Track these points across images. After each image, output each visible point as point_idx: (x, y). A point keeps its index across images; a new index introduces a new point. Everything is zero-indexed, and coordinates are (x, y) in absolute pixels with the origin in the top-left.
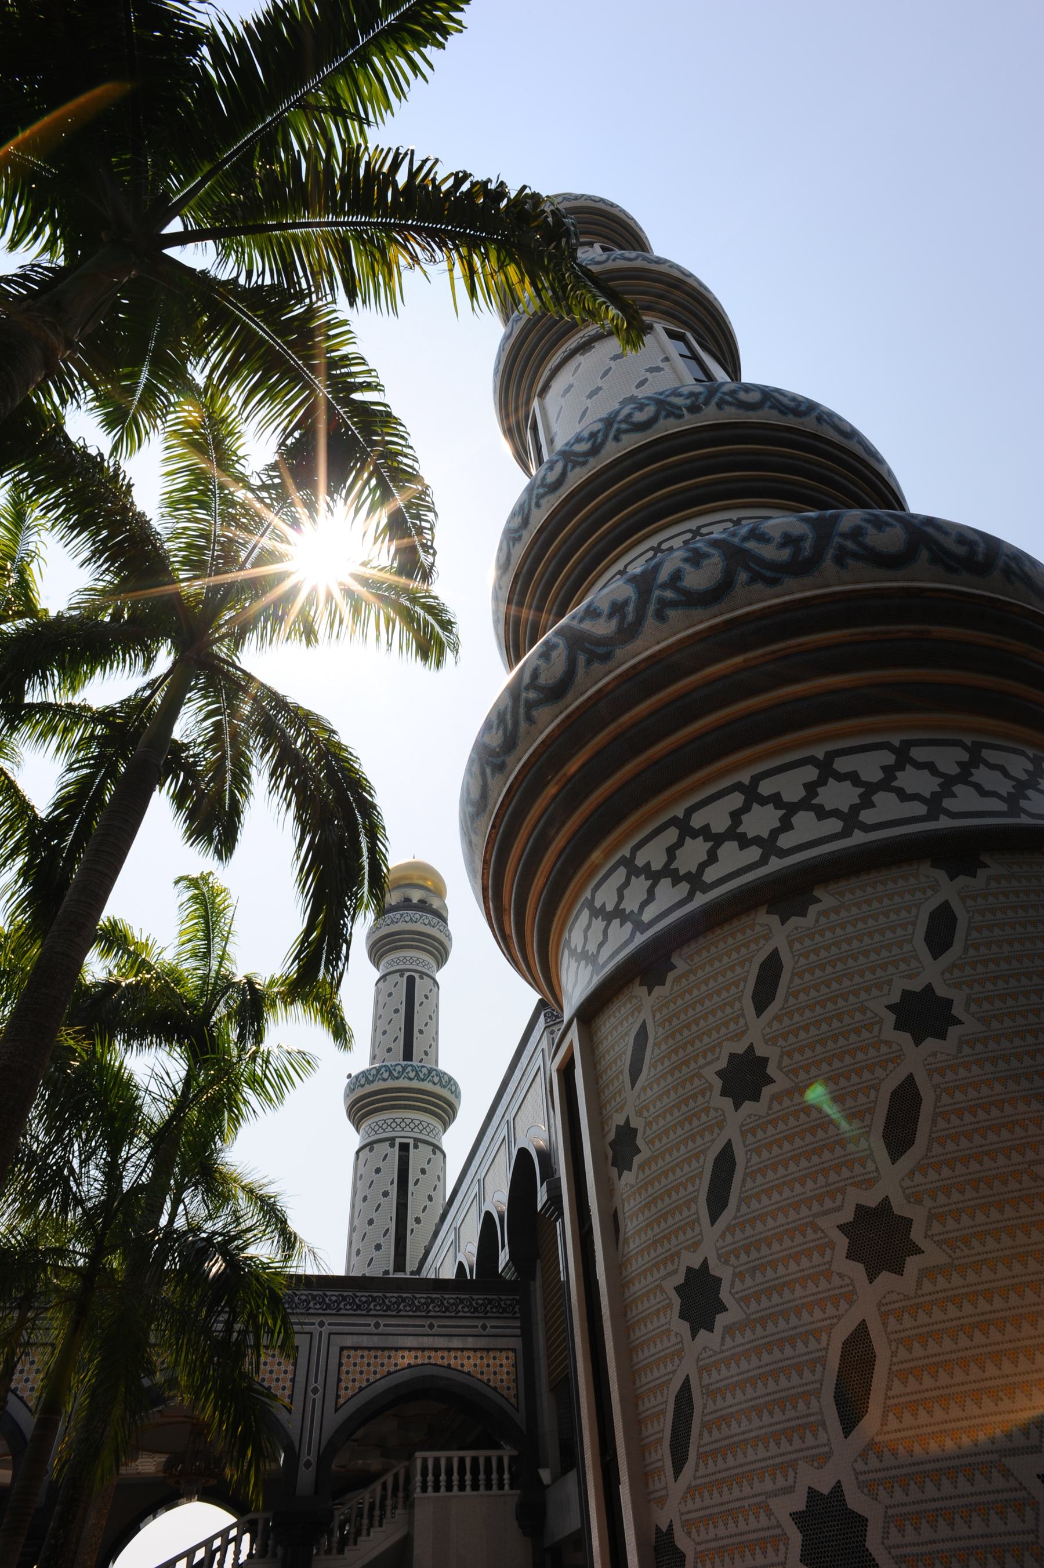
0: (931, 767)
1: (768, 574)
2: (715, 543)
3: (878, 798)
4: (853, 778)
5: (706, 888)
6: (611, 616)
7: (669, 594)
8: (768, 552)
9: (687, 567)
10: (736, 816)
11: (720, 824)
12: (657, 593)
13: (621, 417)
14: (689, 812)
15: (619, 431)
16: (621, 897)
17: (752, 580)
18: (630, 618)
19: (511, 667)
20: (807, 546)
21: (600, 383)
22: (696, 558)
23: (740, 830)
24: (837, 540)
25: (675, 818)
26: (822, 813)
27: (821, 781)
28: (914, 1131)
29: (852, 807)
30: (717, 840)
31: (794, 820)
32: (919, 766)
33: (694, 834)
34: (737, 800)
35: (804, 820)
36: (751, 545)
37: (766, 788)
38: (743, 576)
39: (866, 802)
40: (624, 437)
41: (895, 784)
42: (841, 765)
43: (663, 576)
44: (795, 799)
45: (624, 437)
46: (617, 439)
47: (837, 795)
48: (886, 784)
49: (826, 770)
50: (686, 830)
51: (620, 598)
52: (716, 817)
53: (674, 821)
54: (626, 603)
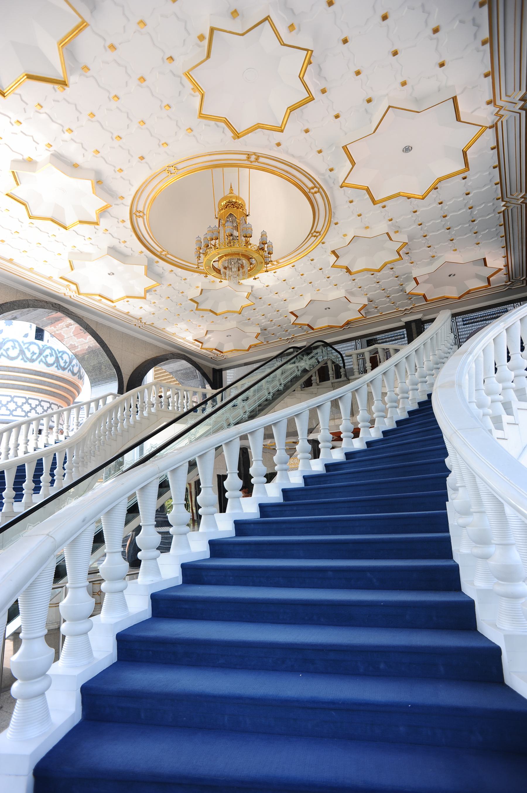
12: (42, 357)
38: (55, 365)
51: (35, 352)
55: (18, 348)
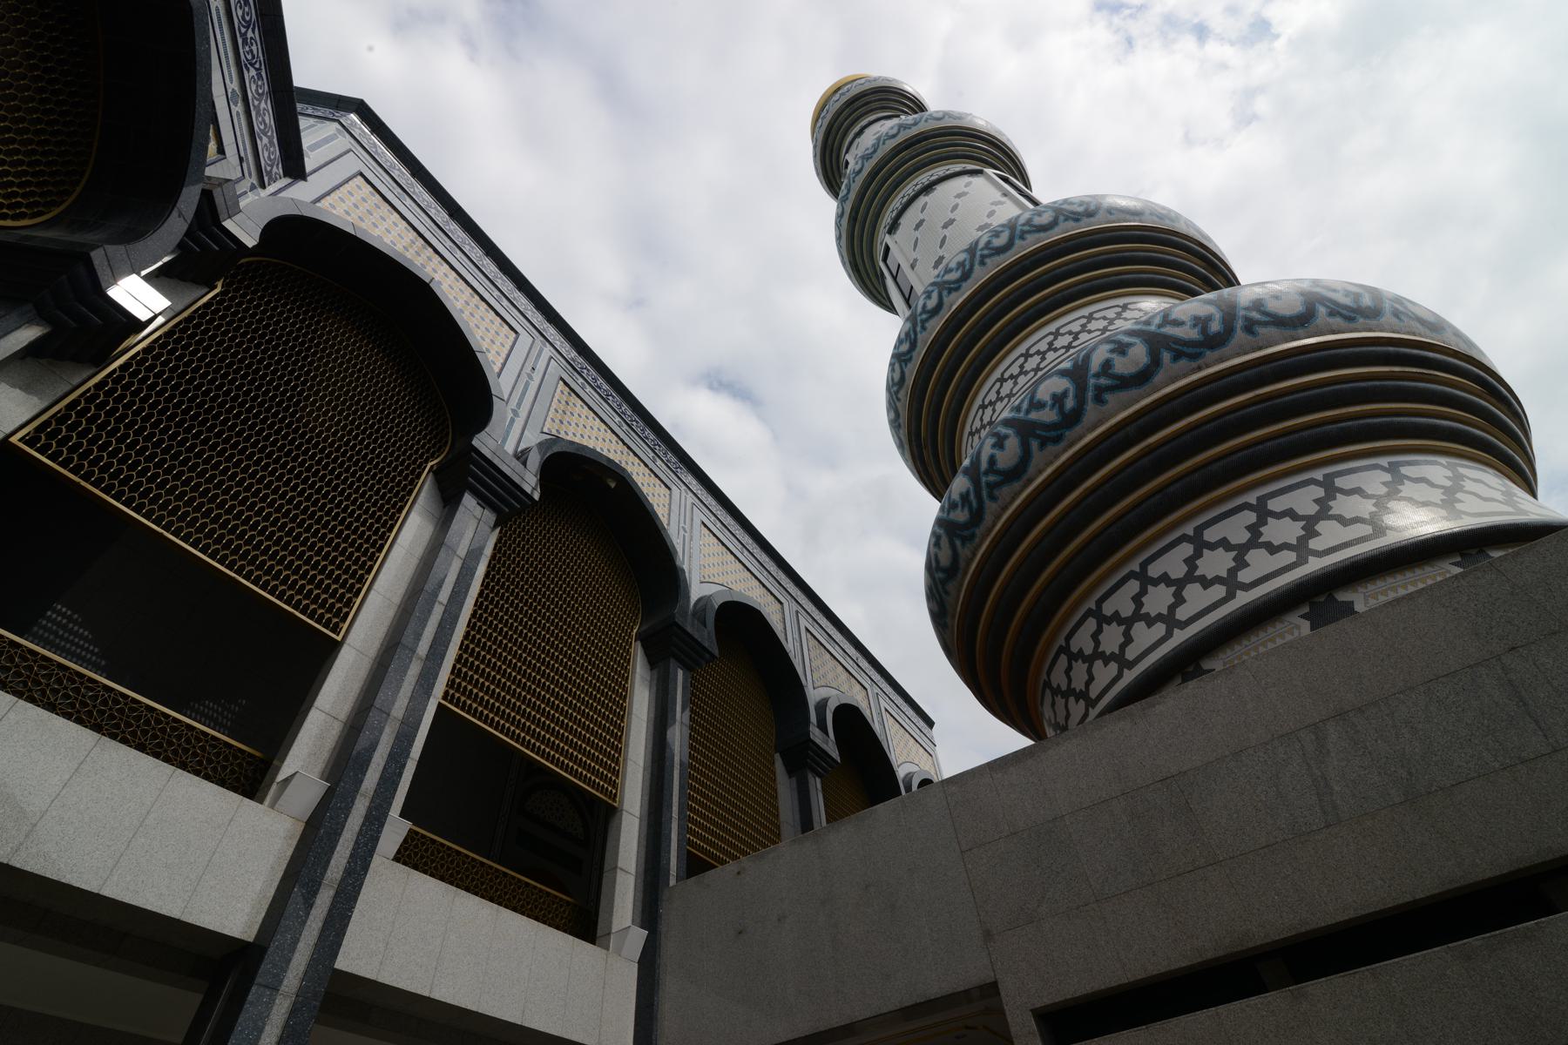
0: (1291, 514)
1: (1053, 434)
2: (1007, 423)
3: (1321, 526)
4: (1224, 544)
5: (1131, 665)
6: (1053, 406)
7: (992, 478)
8: (1048, 416)
9: (1114, 356)
10: (1137, 600)
11: (1178, 571)
13: (981, 245)
14: (1068, 638)
15: (983, 257)
16: (1089, 671)
17: (1042, 445)
18: (975, 504)
19: (585, 924)
20: (1070, 403)
21: (946, 232)
22: (1000, 443)
23: (1197, 573)
24: (1092, 381)
25: (1090, 610)
26: (1206, 583)
27: (1198, 554)
28: (395, 790)
29: (1299, 539)
30: (1128, 623)
31: (1184, 593)
32: (1279, 516)
33: (1109, 620)
34: (1187, 549)
35: (1192, 591)
36: (1033, 416)
37: (1154, 571)
39: (1241, 563)
40: (988, 261)
41: (1234, 553)
42: (1211, 535)
43: (984, 465)
44: (1181, 575)
45: (988, 261)
46: (982, 263)
47: (1216, 563)
48: (1254, 542)
49: (1201, 545)
50: (1103, 620)
51: (1059, 390)
52: (1173, 562)
53: (1089, 613)
54: (1065, 394)
55: (1009, 431)
